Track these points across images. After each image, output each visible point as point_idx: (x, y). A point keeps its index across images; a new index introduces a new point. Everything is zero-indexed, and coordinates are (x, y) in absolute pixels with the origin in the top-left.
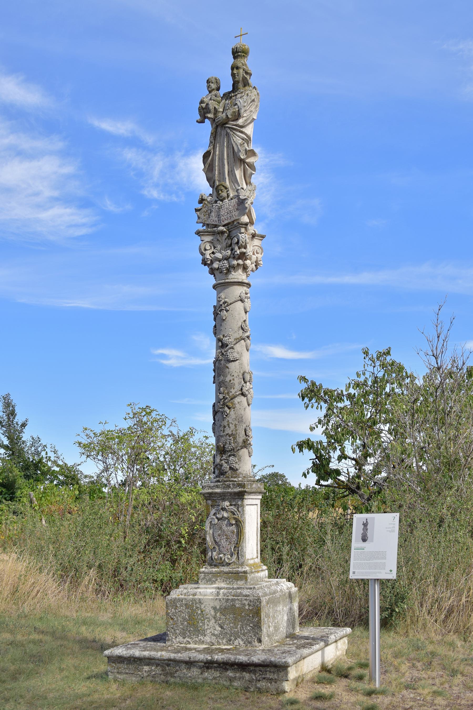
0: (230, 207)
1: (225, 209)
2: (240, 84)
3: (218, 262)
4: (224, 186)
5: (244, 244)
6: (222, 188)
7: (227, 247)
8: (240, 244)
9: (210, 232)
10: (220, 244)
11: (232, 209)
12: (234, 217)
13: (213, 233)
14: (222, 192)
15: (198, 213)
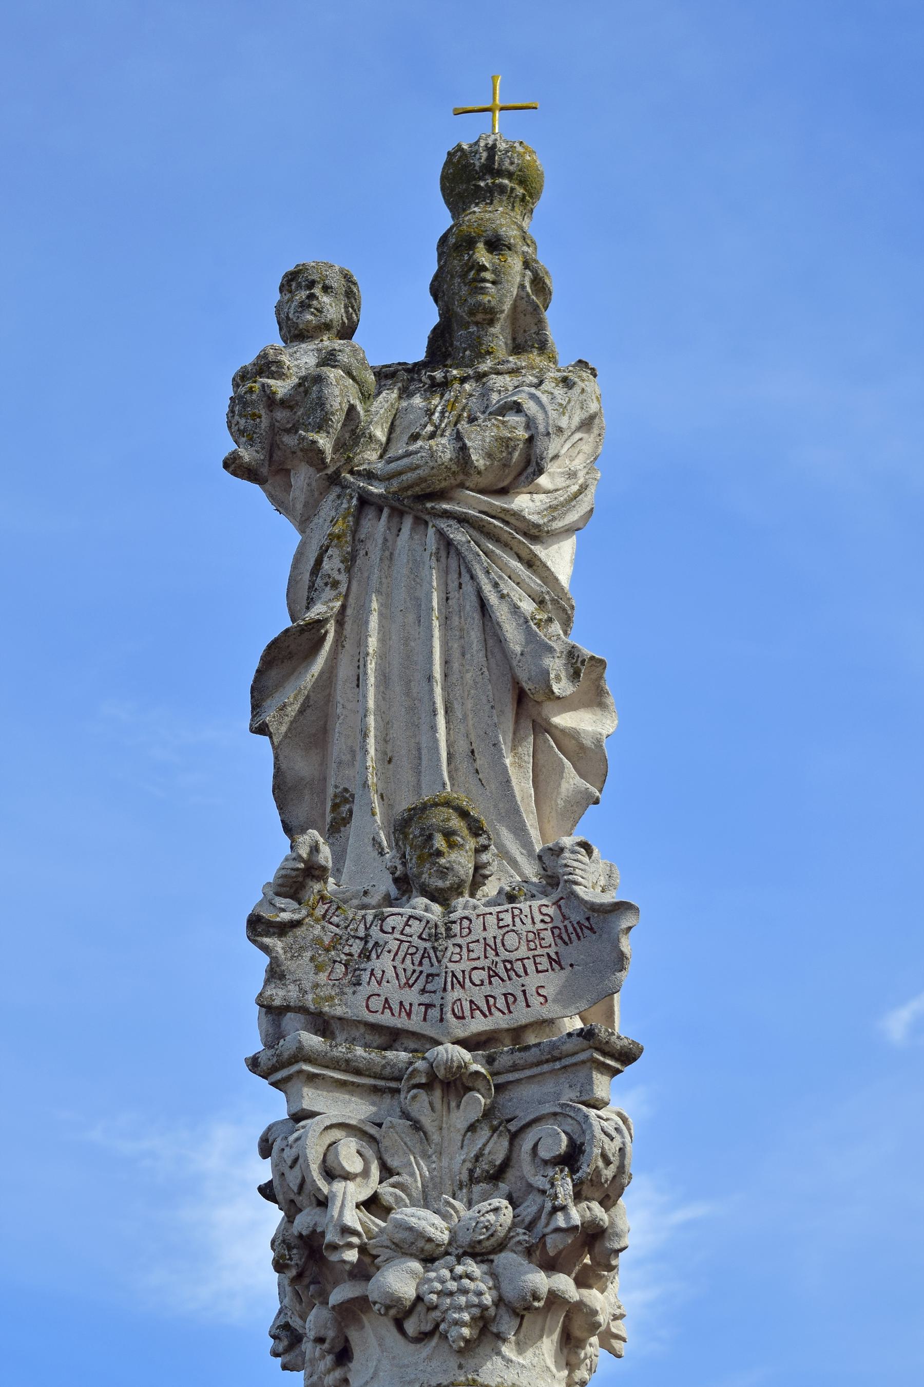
0: (511, 940)
1: (478, 950)
2: (496, 330)
3: (416, 1266)
4: (464, 814)
5: (608, 1173)
6: (456, 823)
7: (473, 1180)
8: (586, 1170)
9: (358, 1072)
10: (426, 1156)
11: (523, 952)
12: (535, 1001)
13: (384, 1085)
14: (452, 845)
15: (276, 944)
